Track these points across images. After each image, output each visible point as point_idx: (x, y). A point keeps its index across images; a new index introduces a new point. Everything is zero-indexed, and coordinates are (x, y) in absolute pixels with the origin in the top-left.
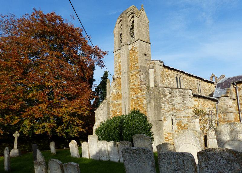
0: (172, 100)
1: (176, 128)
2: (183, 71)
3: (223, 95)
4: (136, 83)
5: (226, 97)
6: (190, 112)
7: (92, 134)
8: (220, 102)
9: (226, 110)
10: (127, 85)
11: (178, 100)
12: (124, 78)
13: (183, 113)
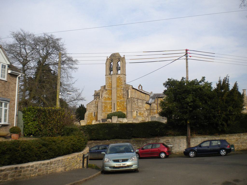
0: (138, 104)
1: (138, 114)
2: (203, 141)
3: (153, 102)
4: (121, 94)
5: (154, 103)
6: (145, 109)
7: (83, 119)
8: (152, 105)
9: (153, 108)
10: (116, 95)
11: (140, 104)
12: (114, 91)
13: (142, 109)
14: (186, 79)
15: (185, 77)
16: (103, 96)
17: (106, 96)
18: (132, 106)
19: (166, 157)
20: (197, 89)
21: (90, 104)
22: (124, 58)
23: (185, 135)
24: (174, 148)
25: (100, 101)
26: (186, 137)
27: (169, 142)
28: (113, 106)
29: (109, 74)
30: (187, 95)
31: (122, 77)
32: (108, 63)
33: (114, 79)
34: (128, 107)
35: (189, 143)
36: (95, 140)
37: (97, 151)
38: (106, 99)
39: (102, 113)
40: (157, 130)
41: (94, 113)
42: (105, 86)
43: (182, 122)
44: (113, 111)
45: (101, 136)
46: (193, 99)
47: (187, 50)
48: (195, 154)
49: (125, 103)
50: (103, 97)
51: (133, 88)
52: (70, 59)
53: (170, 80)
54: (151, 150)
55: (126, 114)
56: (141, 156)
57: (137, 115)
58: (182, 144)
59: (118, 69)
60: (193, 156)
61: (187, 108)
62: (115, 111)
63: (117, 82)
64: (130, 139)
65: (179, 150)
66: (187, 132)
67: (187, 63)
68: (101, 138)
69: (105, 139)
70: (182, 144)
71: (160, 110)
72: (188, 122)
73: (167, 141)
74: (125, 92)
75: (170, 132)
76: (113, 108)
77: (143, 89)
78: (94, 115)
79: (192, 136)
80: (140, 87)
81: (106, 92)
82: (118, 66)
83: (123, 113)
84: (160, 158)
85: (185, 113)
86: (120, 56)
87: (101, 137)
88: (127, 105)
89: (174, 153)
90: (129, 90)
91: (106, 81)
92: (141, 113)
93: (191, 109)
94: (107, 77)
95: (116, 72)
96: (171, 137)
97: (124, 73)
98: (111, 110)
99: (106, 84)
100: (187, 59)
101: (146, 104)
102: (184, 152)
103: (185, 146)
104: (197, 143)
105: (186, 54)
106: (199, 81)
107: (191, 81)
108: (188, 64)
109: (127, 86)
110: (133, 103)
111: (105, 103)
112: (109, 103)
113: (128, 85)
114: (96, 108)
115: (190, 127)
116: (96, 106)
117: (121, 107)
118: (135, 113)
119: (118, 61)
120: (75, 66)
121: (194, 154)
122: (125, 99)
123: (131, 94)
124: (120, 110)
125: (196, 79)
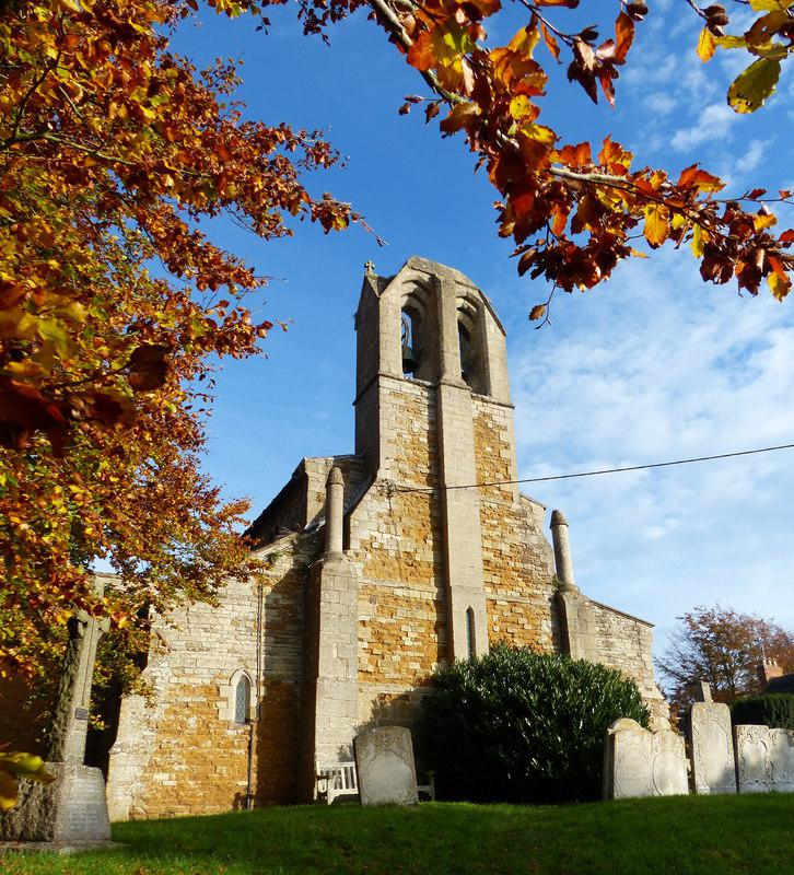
4: (505, 549)
50: (355, 545)
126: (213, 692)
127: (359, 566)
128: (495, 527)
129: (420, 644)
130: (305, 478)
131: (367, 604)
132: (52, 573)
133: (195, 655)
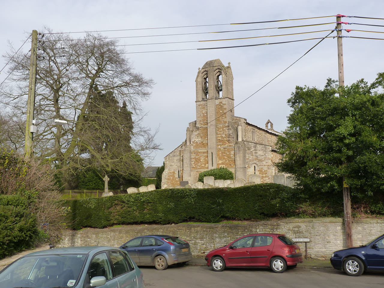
0: (256, 153)
4: (224, 136)
6: (270, 163)
10: (215, 136)
11: (260, 153)
12: (211, 130)
13: (264, 163)
14: (338, 83)
15: (335, 77)
16: (192, 140)
17: (198, 140)
18: (245, 156)
19: (288, 268)
20: (365, 102)
21: (171, 155)
22: (229, 67)
23: (340, 217)
24: (312, 244)
25: (187, 149)
26: (340, 220)
27: (301, 230)
28: (210, 158)
29: (203, 99)
30: (341, 118)
31: (227, 102)
32: (200, 79)
33: (211, 106)
34: (238, 159)
35: (348, 236)
36: (150, 223)
37: (137, 249)
38: (197, 145)
39: (191, 171)
40: (274, 202)
41: (179, 171)
42: (196, 121)
43: (329, 185)
44: (211, 168)
45: (160, 215)
46: (355, 127)
47: (339, 17)
48: (359, 266)
49: (232, 152)
50: (192, 143)
51: (249, 124)
52: (138, 79)
53: (301, 89)
54: (249, 250)
55: (233, 172)
56: (229, 265)
57: (255, 173)
58: (332, 237)
59: (219, 89)
60: (355, 271)
61: (340, 151)
62: (213, 168)
63: (217, 113)
64: (218, 221)
65: (324, 250)
66: (343, 207)
67: (340, 45)
68: (160, 220)
69: (169, 223)
70: (332, 237)
71: (277, 158)
72: (345, 186)
73: (296, 229)
74: (231, 132)
75: (304, 207)
76: (210, 162)
77: (274, 128)
78: (177, 176)
79: (355, 219)
80: (269, 123)
81: (198, 132)
82: (218, 84)
83: (229, 171)
84: (270, 270)
85: (338, 162)
86: (221, 63)
87: (161, 219)
88: (235, 156)
89: (313, 256)
90: (240, 128)
91: (197, 112)
92: (263, 171)
93: (350, 153)
94: (199, 105)
95: (215, 95)
96: (306, 220)
97: (229, 96)
98: (207, 165)
99: (197, 117)
100: (340, 37)
101: (273, 153)
102: (332, 260)
103: (338, 242)
104: (370, 234)
105: (336, 28)
106: (369, 85)
107: (349, 86)
108: (342, 49)
109: (236, 119)
110: (248, 151)
111: (197, 153)
112: (204, 153)
113: (238, 117)
114: (182, 163)
115: (351, 195)
116: (181, 159)
117: (224, 159)
118: (251, 171)
119: (218, 74)
120: (146, 89)
121: (357, 266)
122: (233, 144)
123: (242, 135)
124: (222, 166)
125: (362, 80)
126: (174, 173)
127: (192, 147)
128: (221, 131)
129: (204, 161)
130: (164, 169)
131: (194, 154)
132: (360, 167)
133: (171, 167)
